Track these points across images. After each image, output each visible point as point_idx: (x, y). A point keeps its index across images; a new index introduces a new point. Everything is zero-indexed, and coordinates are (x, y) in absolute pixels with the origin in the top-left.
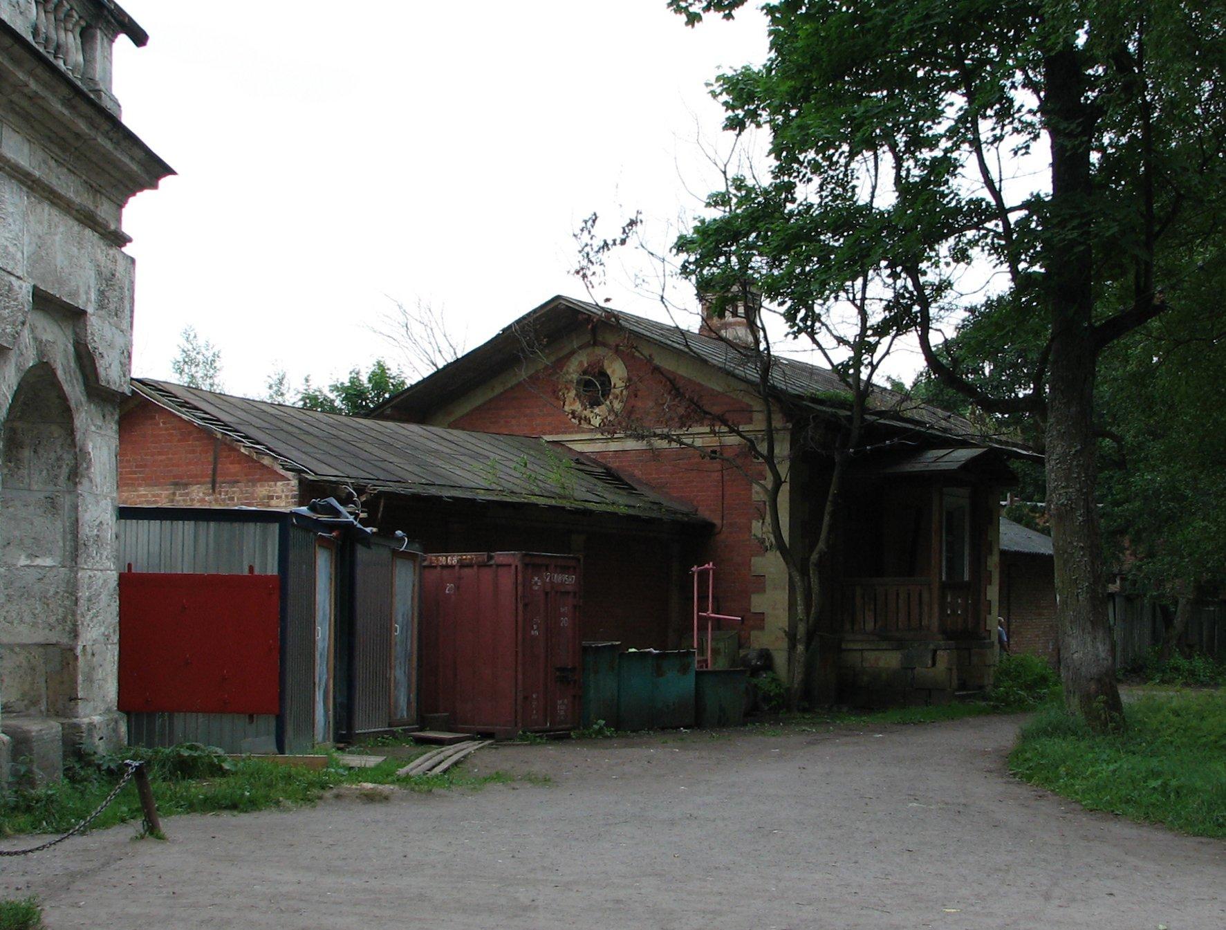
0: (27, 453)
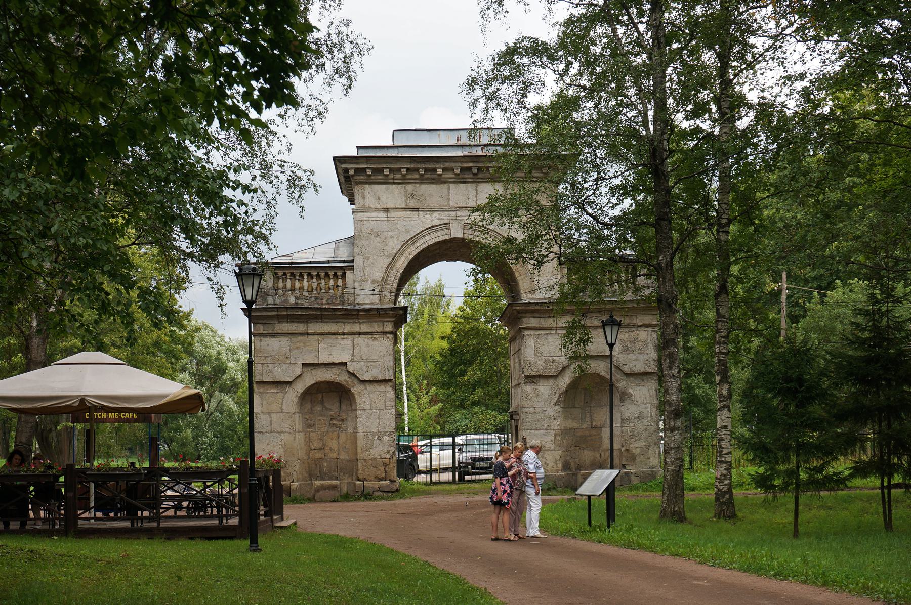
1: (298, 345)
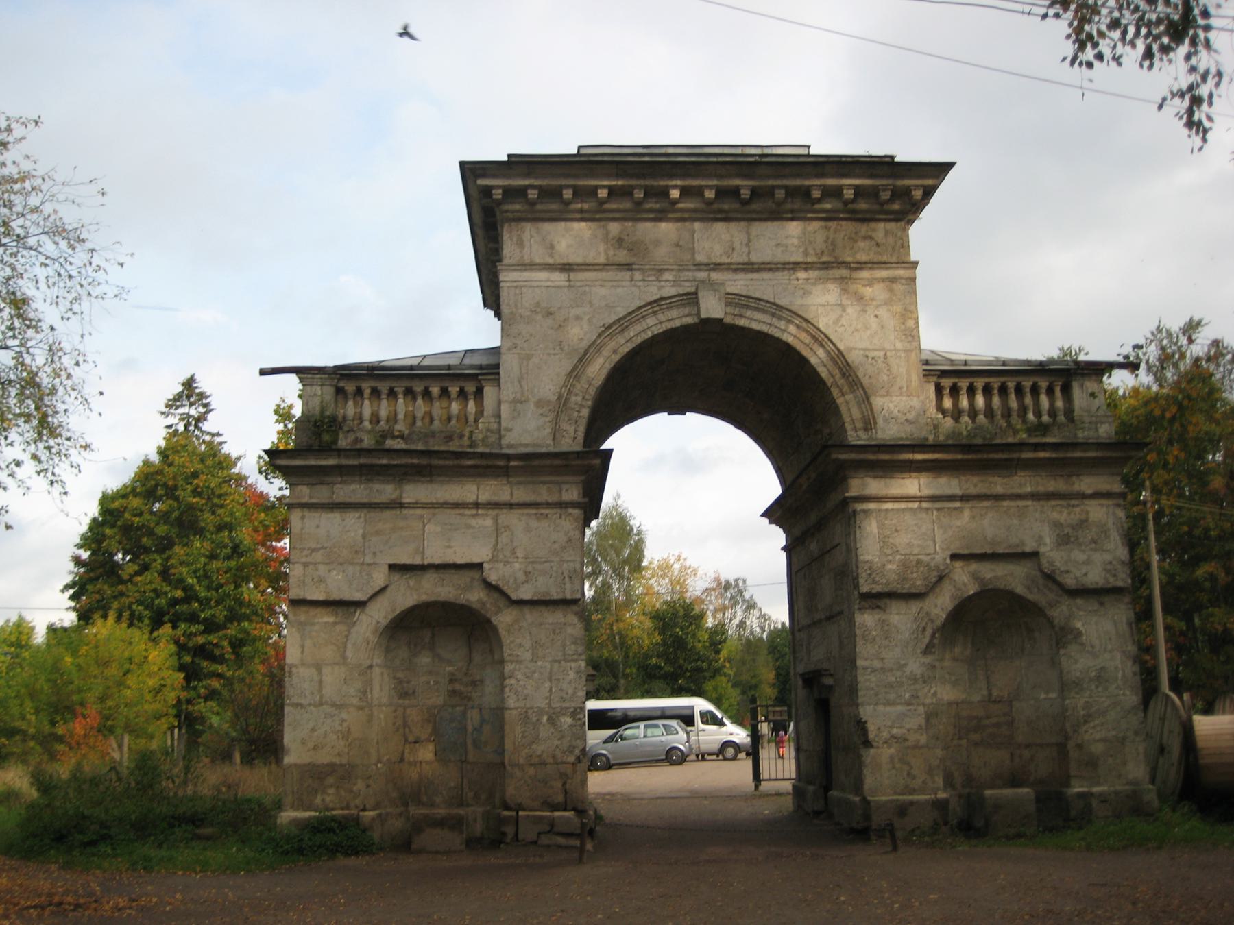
0: (1037, 634)
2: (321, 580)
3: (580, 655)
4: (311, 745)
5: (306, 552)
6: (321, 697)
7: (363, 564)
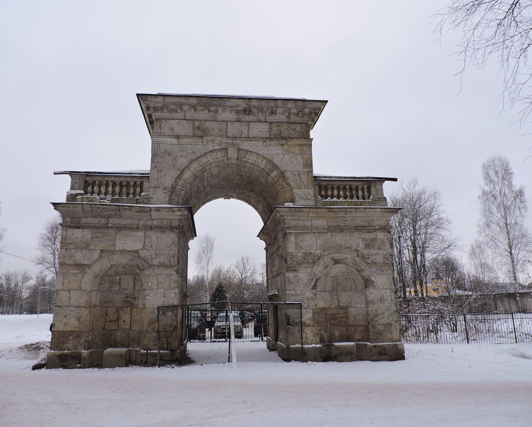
1: (98, 235)
2: (73, 256)
3: (176, 287)
4: (64, 323)
5: (67, 244)
6: (70, 303)
7: (90, 249)
